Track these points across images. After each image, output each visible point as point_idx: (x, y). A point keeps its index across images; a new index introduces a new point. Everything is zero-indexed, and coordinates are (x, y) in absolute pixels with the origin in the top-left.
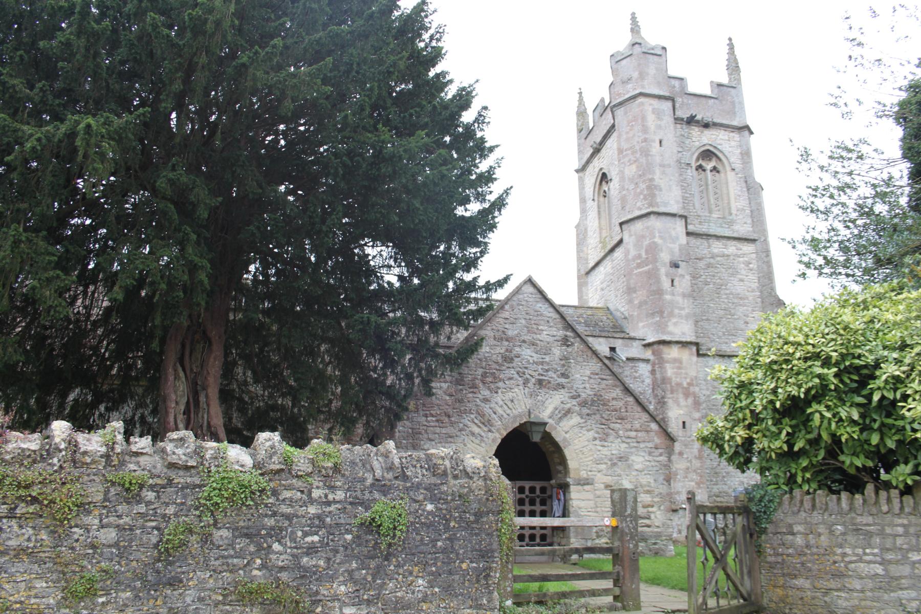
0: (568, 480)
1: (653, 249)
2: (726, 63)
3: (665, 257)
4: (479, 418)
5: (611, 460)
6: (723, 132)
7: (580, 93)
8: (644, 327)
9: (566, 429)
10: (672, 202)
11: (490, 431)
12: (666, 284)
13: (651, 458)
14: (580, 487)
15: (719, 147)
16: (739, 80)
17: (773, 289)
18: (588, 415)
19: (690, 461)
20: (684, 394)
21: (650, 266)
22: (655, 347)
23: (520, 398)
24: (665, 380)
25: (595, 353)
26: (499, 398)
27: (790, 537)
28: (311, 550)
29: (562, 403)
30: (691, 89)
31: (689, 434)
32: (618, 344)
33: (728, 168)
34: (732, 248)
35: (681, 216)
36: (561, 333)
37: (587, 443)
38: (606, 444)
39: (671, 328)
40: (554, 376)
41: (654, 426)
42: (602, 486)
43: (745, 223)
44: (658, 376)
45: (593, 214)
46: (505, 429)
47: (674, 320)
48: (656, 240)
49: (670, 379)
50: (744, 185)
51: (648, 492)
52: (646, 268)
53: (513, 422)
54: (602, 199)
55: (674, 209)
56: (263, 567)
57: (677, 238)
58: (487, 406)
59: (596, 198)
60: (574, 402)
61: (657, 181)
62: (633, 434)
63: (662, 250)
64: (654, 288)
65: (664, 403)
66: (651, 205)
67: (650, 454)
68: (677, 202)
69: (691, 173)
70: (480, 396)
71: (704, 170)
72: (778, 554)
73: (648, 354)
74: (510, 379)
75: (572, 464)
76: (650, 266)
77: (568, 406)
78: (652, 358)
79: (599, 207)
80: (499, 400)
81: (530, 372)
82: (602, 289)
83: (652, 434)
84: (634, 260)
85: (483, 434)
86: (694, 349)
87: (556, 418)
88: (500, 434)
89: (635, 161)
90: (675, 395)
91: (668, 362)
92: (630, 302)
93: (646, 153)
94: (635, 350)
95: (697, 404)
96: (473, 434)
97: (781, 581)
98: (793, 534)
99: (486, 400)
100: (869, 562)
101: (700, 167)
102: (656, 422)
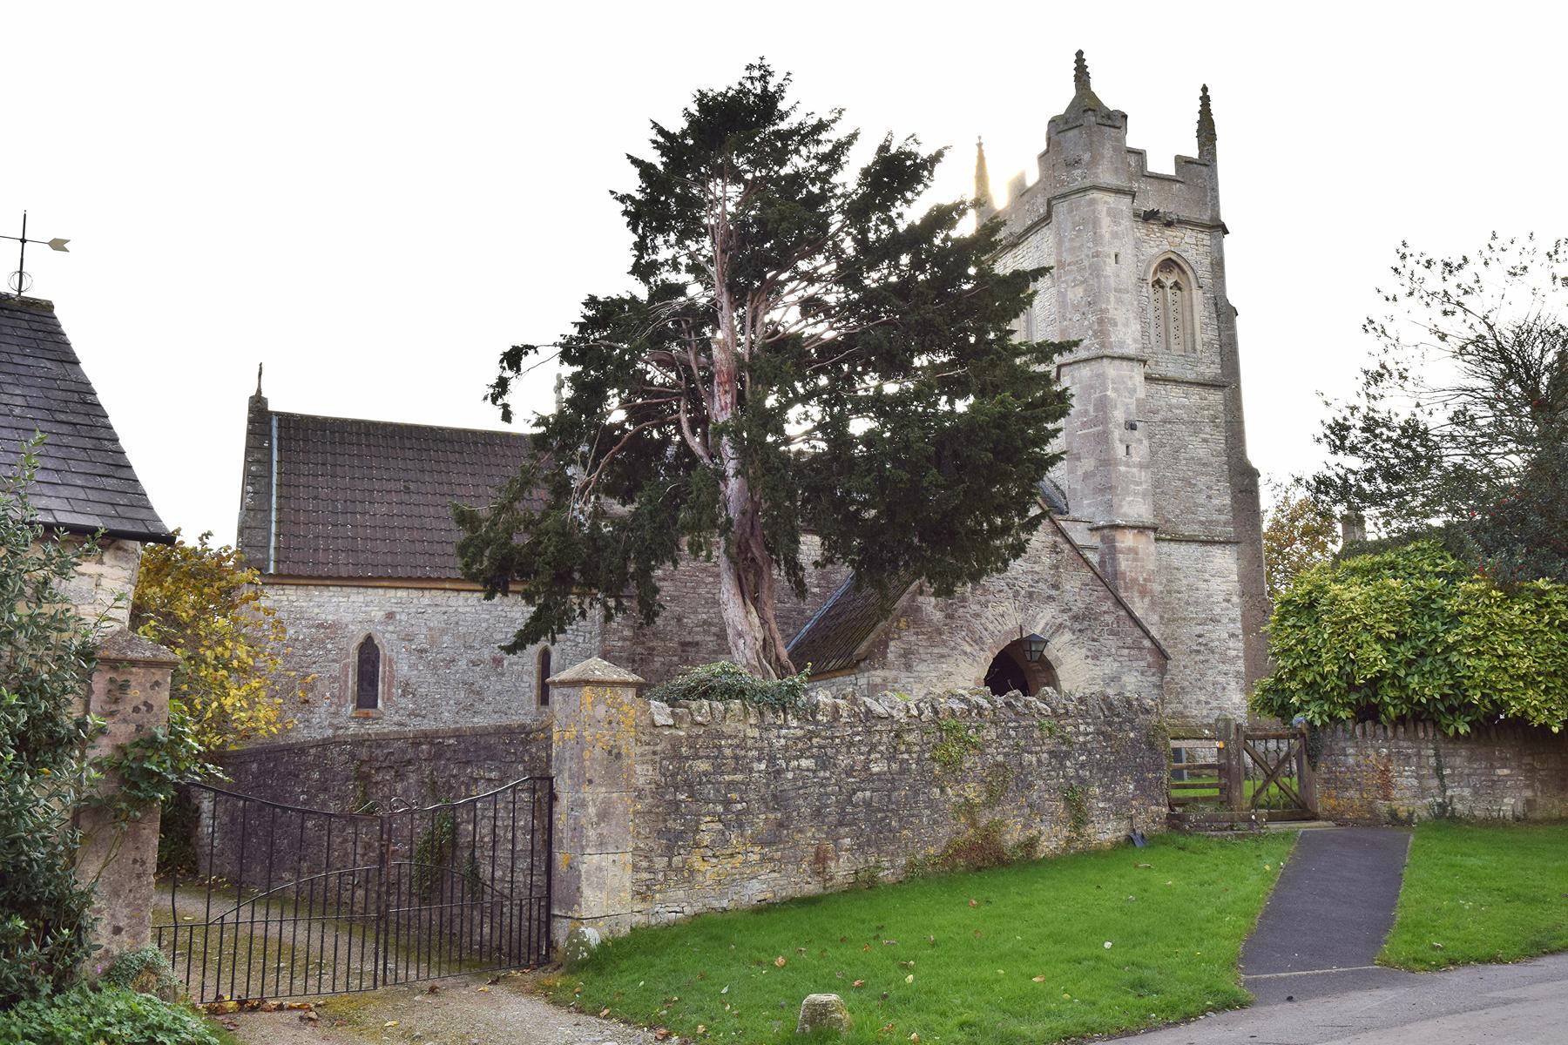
2: (1196, 126)
3: (1119, 415)
6: (1189, 232)
7: (980, 145)
8: (1090, 505)
9: (1058, 646)
10: (1129, 341)
11: (982, 649)
12: (1120, 450)
13: (1143, 678)
15: (1184, 255)
16: (1214, 155)
17: (1243, 453)
21: (1100, 428)
22: (1106, 531)
23: (1011, 611)
25: (1087, 562)
26: (989, 613)
27: (1342, 758)
28: (1083, 766)
30: (1153, 167)
33: (1194, 285)
36: (1051, 539)
39: (1125, 509)
40: (1044, 587)
41: (1147, 643)
43: (1213, 363)
49: (1123, 574)
50: (1213, 309)
55: (1131, 349)
56: (1064, 776)
60: (1065, 617)
61: (1112, 313)
62: (1126, 652)
64: (1103, 456)
66: (1103, 345)
67: (1142, 673)
68: (1135, 341)
69: (1148, 290)
71: (1162, 287)
72: (399, 880)
74: (1001, 591)
76: (1100, 428)
78: (1100, 545)
83: (1145, 652)
89: (1082, 282)
91: (1121, 552)
93: (1096, 271)
96: (965, 653)
97: (1334, 793)
98: (1346, 755)
99: (977, 616)
100: (1407, 777)
101: (1158, 282)
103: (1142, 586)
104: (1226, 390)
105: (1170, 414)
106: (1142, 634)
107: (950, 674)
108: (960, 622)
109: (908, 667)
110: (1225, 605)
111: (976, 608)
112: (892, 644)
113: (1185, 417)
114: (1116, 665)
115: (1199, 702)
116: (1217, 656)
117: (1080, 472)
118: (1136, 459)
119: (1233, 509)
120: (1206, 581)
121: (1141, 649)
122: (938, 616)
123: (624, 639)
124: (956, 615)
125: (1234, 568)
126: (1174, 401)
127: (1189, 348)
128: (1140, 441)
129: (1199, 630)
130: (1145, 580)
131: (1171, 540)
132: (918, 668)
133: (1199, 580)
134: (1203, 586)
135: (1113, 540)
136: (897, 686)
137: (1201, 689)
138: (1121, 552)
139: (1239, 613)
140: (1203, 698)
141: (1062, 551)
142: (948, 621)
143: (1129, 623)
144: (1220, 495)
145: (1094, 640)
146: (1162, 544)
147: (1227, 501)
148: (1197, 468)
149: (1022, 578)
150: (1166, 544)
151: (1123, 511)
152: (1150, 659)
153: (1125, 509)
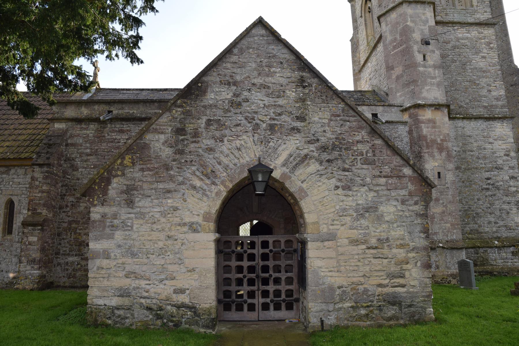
0: (305, 235)
1: (406, 32)
3: (417, 36)
4: (201, 169)
5: (356, 211)
8: (401, 96)
9: (302, 178)
11: (214, 183)
12: (419, 58)
13: (404, 208)
14: (319, 244)
17: (512, 61)
18: (328, 161)
19: (446, 206)
20: (439, 149)
21: (404, 46)
22: (412, 111)
24: (421, 137)
26: (225, 147)
29: (297, 149)
31: (443, 182)
32: (379, 110)
34: (474, 32)
35: (429, 3)
37: (327, 193)
38: (350, 193)
39: (425, 94)
40: (288, 119)
41: (407, 171)
42: (346, 241)
43: (486, 12)
44: (415, 134)
45: (362, 28)
46: (231, 181)
47: (427, 88)
48: (408, 23)
49: (425, 137)
51: (401, 246)
52: (401, 48)
53: (239, 174)
54: (367, 14)
57: (427, 21)
58: (211, 156)
59: (363, 15)
60: (312, 147)
62: (383, 181)
63: (414, 31)
64: (407, 63)
65: (421, 157)
67: (403, 202)
70: (203, 146)
73: (406, 117)
74: (238, 125)
75: (309, 218)
76: (404, 46)
77: (305, 151)
79: (365, 21)
80: (224, 149)
81: (260, 117)
82: (370, 79)
84: (390, 44)
85: (205, 187)
86: (446, 111)
87: (291, 166)
88: (225, 186)
90: (430, 150)
91: (423, 122)
92: (389, 78)
94: (393, 115)
95: (449, 156)
96: (194, 188)
99: (210, 150)
102: (410, 165)
103: (440, 144)
104: (496, 26)
105: (458, 43)
106: (402, 162)
107: (176, 209)
108: (189, 158)
109: (130, 203)
110: (505, 158)
111: (210, 142)
112: (115, 180)
113: (469, 44)
114: (371, 194)
115: (489, 223)
116: (501, 191)
117: (394, 77)
118: (430, 62)
119: (507, 97)
120: (490, 143)
121: (399, 177)
122: (167, 152)
123: (43, 192)
124: (187, 150)
125: (511, 134)
126: (460, 35)
127: (469, 4)
128: (433, 52)
129: (487, 175)
130: (442, 140)
131: (463, 118)
132: (140, 204)
133: (485, 142)
134: (490, 146)
135: (417, 115)
136: (116, 222)
137: (490, 214)
138: (423, 122)
139: (516, 163)
140: (493, 220)
141: (310, 85)
142: (178, 156)
143: (386, 153)
144: (497, 89)
145: (344, 170)
146: (457, 121)
147: (502, 92)
148: (479, 74)
149: (263, 112)
150: (460, 121)
151: (423, 95)
152: (411, 187)
153: (425, 94)
